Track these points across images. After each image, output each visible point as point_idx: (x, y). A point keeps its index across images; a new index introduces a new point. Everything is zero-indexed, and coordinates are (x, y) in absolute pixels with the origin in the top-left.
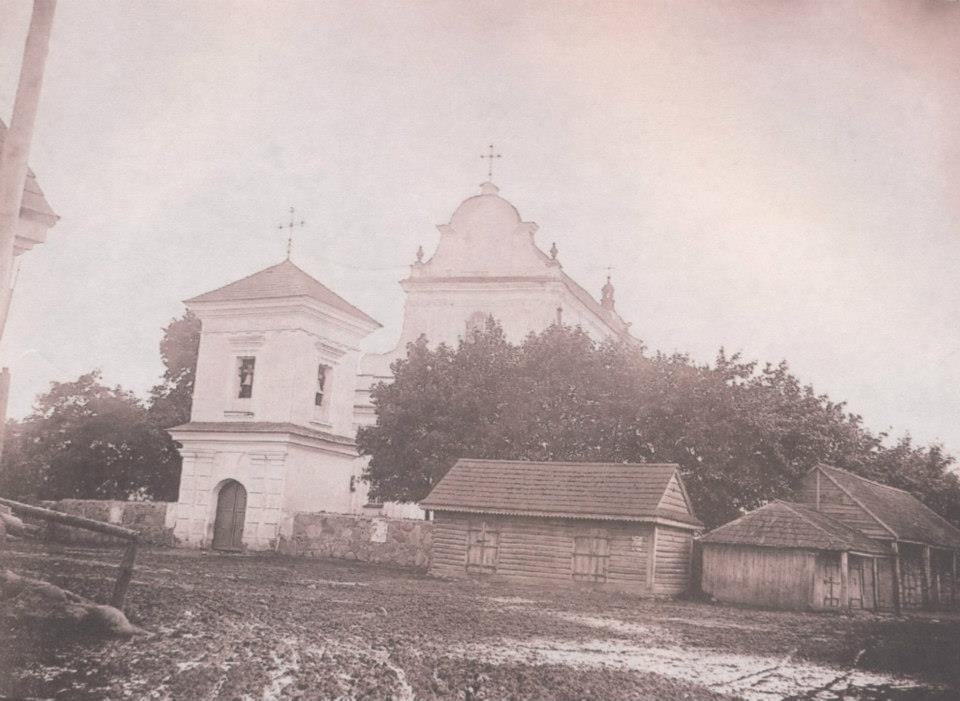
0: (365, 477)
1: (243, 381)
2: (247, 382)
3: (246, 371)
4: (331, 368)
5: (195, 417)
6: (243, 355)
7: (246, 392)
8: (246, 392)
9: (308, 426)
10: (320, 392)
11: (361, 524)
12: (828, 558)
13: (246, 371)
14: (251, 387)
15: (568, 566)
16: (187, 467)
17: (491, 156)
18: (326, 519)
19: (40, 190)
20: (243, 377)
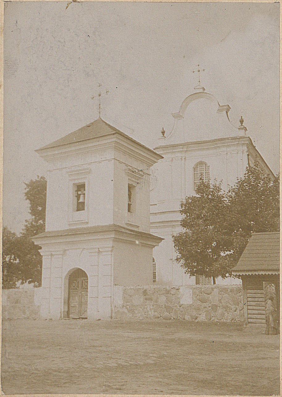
0: (32, 216)
1: (78, 200)
2: (81, 200)
3: (79, 193)
4: (134, 187)
5: (49, 228)
6: (76, 182)
7: (80, 207)
8: (80, 207)
9: (126, 226)
10: (130, 203)
11: (173, 292)
12: (18, 368)
13: (79, 193)
14: (84, 203)
15: (250, 311)
16: (46, 262)
17: (199, 71)
18: (146, 290)
19: (128, 192)
20: (78, 197)
